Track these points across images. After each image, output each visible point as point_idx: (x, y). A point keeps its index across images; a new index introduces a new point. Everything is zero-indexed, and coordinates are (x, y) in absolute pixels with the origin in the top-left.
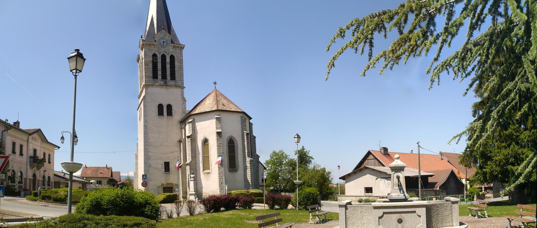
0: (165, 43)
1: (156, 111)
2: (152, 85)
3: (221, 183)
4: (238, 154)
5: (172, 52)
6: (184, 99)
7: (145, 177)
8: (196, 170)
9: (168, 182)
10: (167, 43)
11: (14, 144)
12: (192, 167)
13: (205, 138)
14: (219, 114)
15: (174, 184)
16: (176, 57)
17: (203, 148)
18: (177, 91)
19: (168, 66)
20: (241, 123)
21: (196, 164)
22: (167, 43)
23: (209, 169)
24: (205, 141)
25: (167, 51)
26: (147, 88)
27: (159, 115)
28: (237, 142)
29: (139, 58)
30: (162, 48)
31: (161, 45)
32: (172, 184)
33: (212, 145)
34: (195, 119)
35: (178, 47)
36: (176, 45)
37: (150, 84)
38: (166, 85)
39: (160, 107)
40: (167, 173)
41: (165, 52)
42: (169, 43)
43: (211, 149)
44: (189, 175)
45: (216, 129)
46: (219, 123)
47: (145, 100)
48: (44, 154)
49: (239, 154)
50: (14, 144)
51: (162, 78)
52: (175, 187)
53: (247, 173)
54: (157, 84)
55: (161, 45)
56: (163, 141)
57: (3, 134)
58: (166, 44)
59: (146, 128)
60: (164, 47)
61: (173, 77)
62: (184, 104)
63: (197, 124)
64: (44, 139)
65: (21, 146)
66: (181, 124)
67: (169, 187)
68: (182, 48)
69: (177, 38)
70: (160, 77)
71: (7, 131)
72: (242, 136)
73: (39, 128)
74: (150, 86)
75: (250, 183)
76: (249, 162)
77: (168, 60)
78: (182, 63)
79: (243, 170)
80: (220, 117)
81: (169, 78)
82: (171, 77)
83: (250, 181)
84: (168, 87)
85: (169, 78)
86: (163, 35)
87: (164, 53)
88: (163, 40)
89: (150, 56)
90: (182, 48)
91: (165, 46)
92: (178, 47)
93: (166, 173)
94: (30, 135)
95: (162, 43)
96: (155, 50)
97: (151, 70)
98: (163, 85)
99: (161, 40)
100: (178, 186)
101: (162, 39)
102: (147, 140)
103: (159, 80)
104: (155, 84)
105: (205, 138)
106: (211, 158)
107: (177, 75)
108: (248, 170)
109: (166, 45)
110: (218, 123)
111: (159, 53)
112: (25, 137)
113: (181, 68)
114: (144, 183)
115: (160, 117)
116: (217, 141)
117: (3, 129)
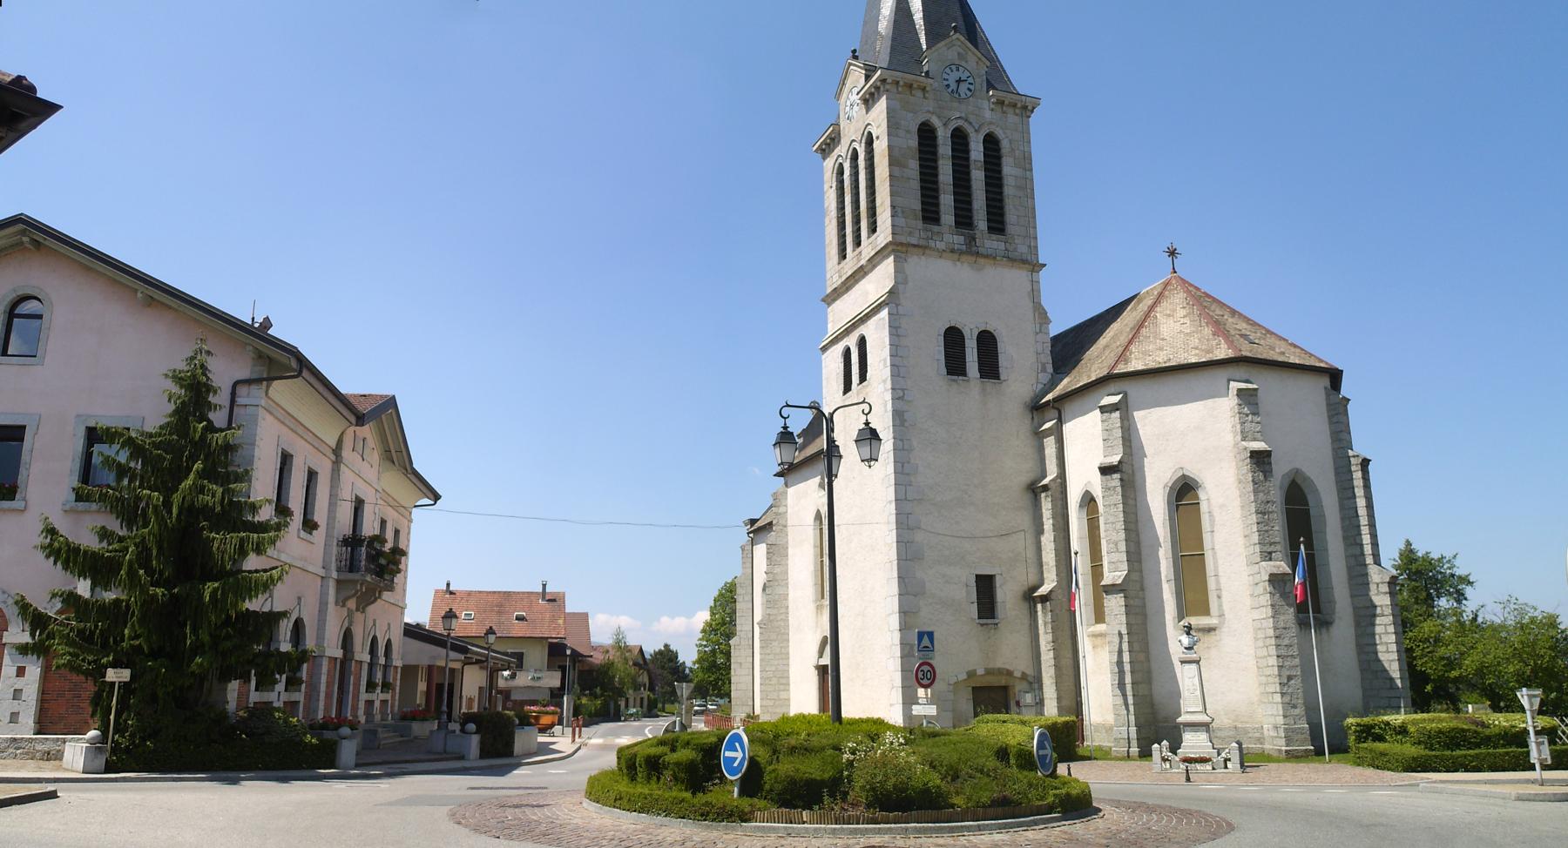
0: (963, 87)
1: (936, 357)
2: (922, 248)
3: (1290, 678)
4: (1327, 550)
5: (991, 123)
6: (1040, 313)
7: (926, 642)
8: (1145, 615)
9: (991, 666)
10: (971, 87)
11: (286, 460)
12: (1132, 602)
13: (1184, 475)
14: (1244, 378)
15: (1018, 674)
16: (1005, 145)
17: (1171, 519)
18: (1019, 276)
19: (978, 177)
20: (1330, 417)
21: (1142, 589)
22: (971, 87)
23: (1206, 611)
24: (1184, 492)
25: (972, 118)
26: (903, 255)
27: (948, 373)
28: (1319, 501)
29: (833, 139)
30: (956, 104)
31: (950, 90)
32: (1009, 673)
33: (1222, 506)
34: (1129, 393)
35: (1015, 106)
36: (1008, 98)
37: (914, 241)
38: (971, 250)
39: (953, 338)
40: (987, 624)
41: (966, 120)
42: (978, 86)
43: (1212, 525)
44: (1120, 634)
45: (1244, 439)
46: (1254, 414)
47: (897, 305)
48: (383, 522)
49: (1331, 552)
50: (286, 460)
51: (958, 224)
52: (1019, 686)
53: (1377, 637)
54: (941, 245)
55: (950, 90)
56: (968, 485)
57: (240, 401)
58: (969, 89)
59: (902, 424)
60: (960, 100)
61: (997, 224)
62: (1040, 331)
63: (1138, 415)
64: (397, 454)
65: (312, 475)
66: (1035, 413)
67: (996, 685)
68: (1030, 108)
69: (1004, 71)
70: (948, 218)
71: (265, 383)
72: (1337, 473)
73: (388, 392)
74: (916, 250)
75: (1399, 682)
76: (1385, 588)
77: (977, 152)
78: (1027, 166)
79: (1353, 624)
80: (1255, 386)
81: (981, 223)
82: (989, 220)
83: (1396, 674)
84: (982, 261)
85: (981, 223)
86: (956, 54)
87: (960, 123)
88: (954, 76)
89: (908, 132)
90: (1025, 108)
91: (963, 96)
92: (1015, 106)
93: (982, 625)
94: (361, 419)
95: (953, 86)
96: (925, 110)
97: (915, 185)
98: (961, 253)
99: (948, 70)
100: (1035, 683)
101: (954, 67)
102: (908, 474)
103: (945, 229)
104: (932, 243)
105: (1184, 475)
106: (1216, 563)
107: (1011, 216)
108: (1378, 620)
109: (968, 93)
110: (1247, 415)
111: (945, 120)
112: (328, 428)
113: (1027, 187)
114: (926, 668)
115: (954, 380)
116: (1256, 492)
117: (244, 373)
